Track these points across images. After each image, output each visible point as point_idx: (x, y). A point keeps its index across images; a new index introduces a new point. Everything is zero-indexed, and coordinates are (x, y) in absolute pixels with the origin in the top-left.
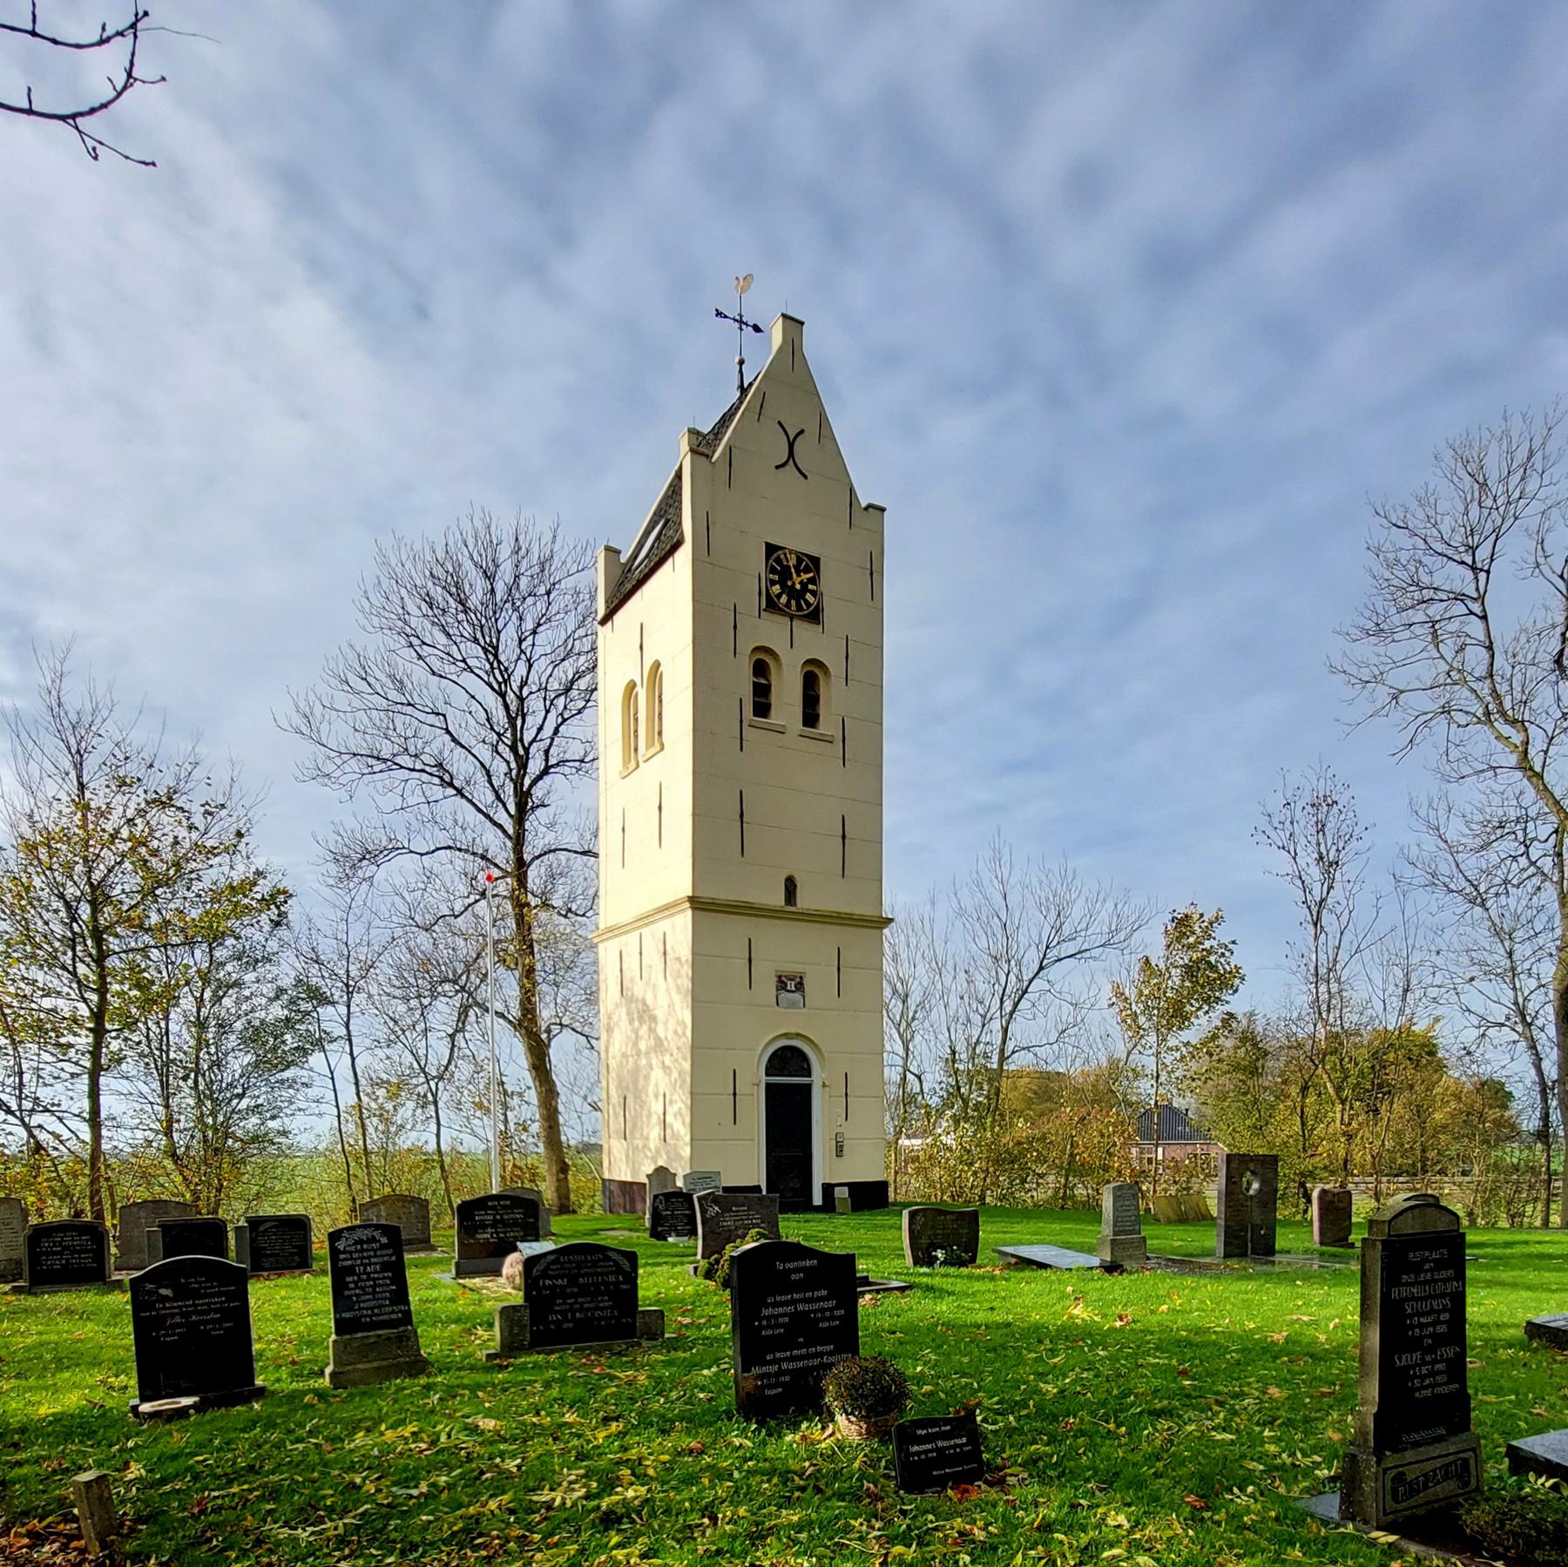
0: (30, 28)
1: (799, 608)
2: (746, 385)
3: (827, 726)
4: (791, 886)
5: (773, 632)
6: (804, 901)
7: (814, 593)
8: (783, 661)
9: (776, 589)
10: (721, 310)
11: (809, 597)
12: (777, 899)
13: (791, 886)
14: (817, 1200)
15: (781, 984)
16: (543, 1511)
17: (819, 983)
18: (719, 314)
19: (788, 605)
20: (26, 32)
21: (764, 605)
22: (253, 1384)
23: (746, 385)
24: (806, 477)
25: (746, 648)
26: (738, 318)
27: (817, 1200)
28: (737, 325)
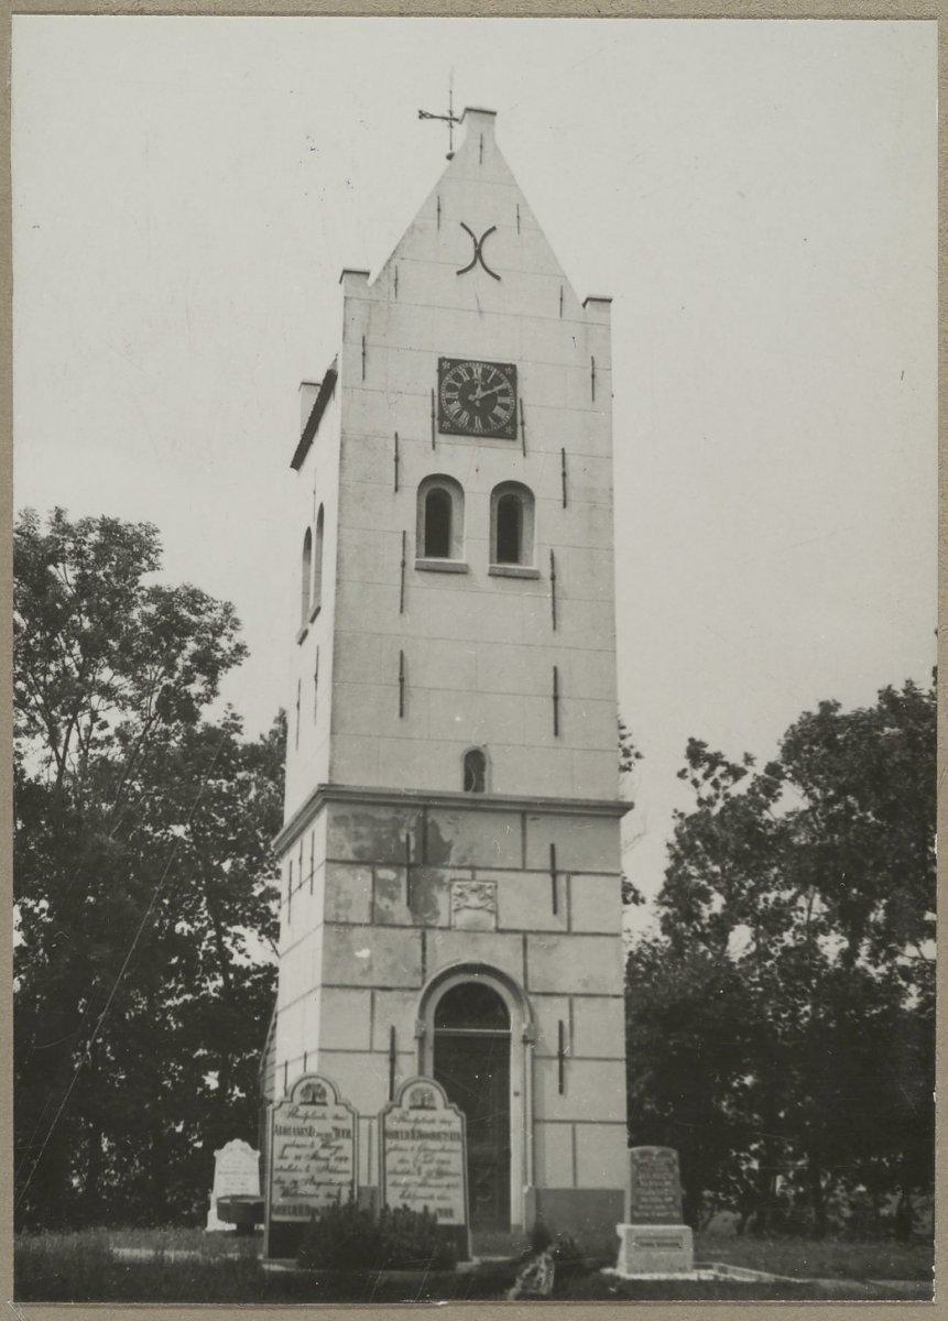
0: (578, 1126)
1: (486, 424)
2: (478, 242)
3: (535, 557)
4: (475, 763)
6: (500, 784)
7: (505, 407)
8: (465, 490)
9: (455, 407)
10: (425, 110)
11: (498, 410)
12: (529, 937)
13: (475, 763)
16: (281, 736)
18: (422, 115)
19: (471, 423)
20: (480, 869)
21: (437, 429)
22: (453, 1269)
23: (478, 242)
24: (498, 278)
25: (414, 474)
26: (448, 115)
28: (446, 123)
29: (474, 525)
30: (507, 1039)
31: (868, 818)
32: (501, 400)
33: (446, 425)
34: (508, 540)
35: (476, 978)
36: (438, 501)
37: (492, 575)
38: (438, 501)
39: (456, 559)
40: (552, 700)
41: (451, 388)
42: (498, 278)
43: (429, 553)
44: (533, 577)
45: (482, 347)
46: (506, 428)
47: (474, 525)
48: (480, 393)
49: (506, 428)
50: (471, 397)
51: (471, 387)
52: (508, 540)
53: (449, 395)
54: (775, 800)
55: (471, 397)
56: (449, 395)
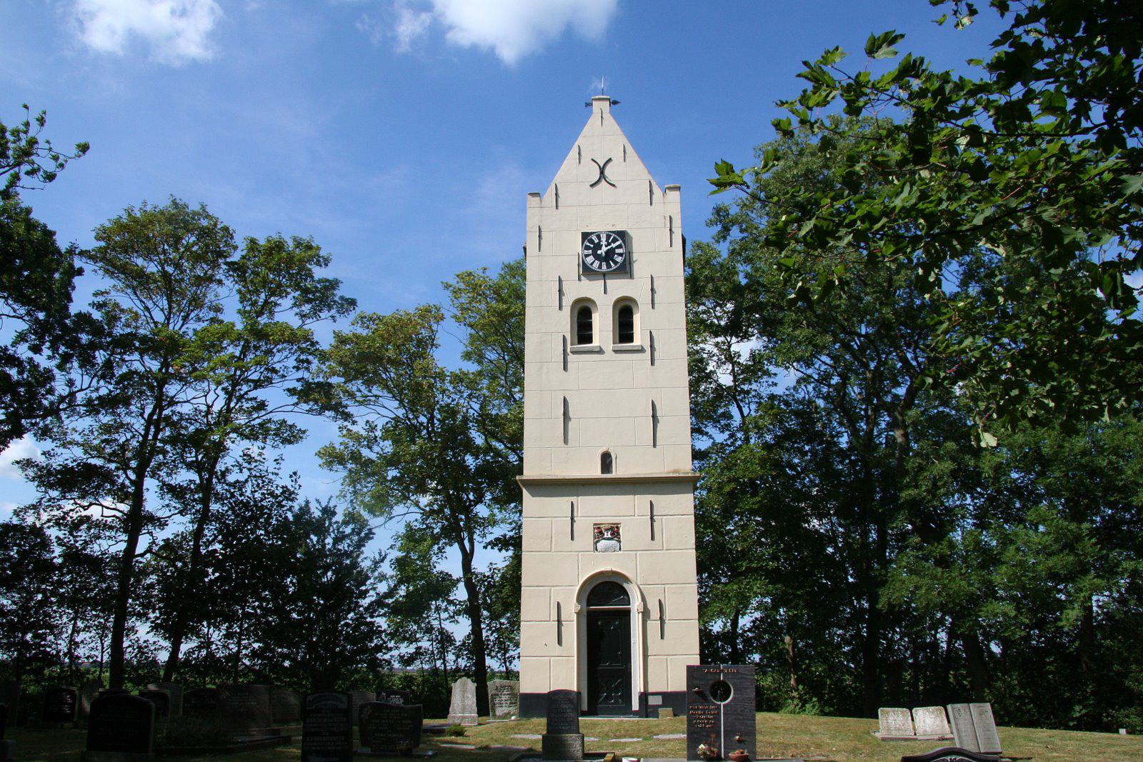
3: (639, 338)
4: (606, 462)
5: (591, 289)
9: (590, 259)
13: (606, 462)
14: (635, 706)
15: (599, 533)
17: (635, 529)
18: (970, 62)
24: (613, 185)
25: (568, 301)
27: (635, 706)
29: (603, 324)
30: (627, 613)
31: (154, 612)
32: (618, 251)
33: (587, 271)
34: (624, 331)
35: (612, 580)
36: (583, 316)
37: (616, 351)
38: (583, 316)
39: (596, 342)
40: (571, 414)
41: (587, 248)
42: (613, 185)
43: (580, 342)
44: (642, 350)
45: (602, 224)
46: (625, 270)
47: (603, 324)
48: (604, 249)
49: (625, 270)
50: (599, 252)
51: (599, 246)
52: (624, 331)
53: (586, 252)
54: (168, 539)
55: (599, 252)
56: (586, 252)
